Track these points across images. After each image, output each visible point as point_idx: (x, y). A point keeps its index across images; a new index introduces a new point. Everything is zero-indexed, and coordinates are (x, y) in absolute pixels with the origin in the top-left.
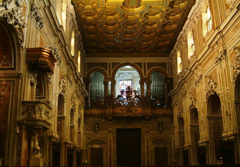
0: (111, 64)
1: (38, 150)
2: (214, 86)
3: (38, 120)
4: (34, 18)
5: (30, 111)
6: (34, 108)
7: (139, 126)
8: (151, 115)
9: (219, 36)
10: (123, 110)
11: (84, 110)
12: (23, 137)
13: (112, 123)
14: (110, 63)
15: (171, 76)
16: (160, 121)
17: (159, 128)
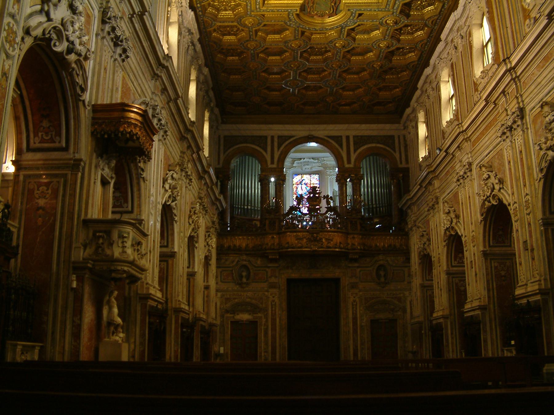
0: (276, 139)
1: (117, 326)
2: (497, 187)
3: (118, 261)
4: (108, 38)
5: (101, 241)
6: (108, 233)
7: (335, 273)
8: (361, 249)
9: (508, 79)
10: (302, 239)
11: (218, 240)
12: (86, 297)
13: (277, 267)
14: (272, 137)
15: (404, 165)
16: (381, 262)
17: (378, 276)
